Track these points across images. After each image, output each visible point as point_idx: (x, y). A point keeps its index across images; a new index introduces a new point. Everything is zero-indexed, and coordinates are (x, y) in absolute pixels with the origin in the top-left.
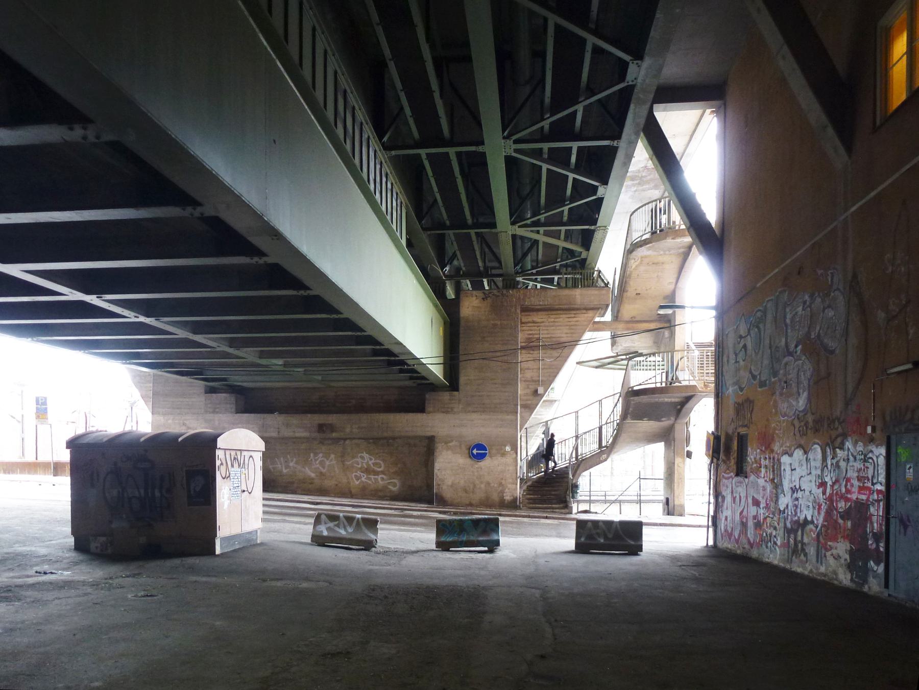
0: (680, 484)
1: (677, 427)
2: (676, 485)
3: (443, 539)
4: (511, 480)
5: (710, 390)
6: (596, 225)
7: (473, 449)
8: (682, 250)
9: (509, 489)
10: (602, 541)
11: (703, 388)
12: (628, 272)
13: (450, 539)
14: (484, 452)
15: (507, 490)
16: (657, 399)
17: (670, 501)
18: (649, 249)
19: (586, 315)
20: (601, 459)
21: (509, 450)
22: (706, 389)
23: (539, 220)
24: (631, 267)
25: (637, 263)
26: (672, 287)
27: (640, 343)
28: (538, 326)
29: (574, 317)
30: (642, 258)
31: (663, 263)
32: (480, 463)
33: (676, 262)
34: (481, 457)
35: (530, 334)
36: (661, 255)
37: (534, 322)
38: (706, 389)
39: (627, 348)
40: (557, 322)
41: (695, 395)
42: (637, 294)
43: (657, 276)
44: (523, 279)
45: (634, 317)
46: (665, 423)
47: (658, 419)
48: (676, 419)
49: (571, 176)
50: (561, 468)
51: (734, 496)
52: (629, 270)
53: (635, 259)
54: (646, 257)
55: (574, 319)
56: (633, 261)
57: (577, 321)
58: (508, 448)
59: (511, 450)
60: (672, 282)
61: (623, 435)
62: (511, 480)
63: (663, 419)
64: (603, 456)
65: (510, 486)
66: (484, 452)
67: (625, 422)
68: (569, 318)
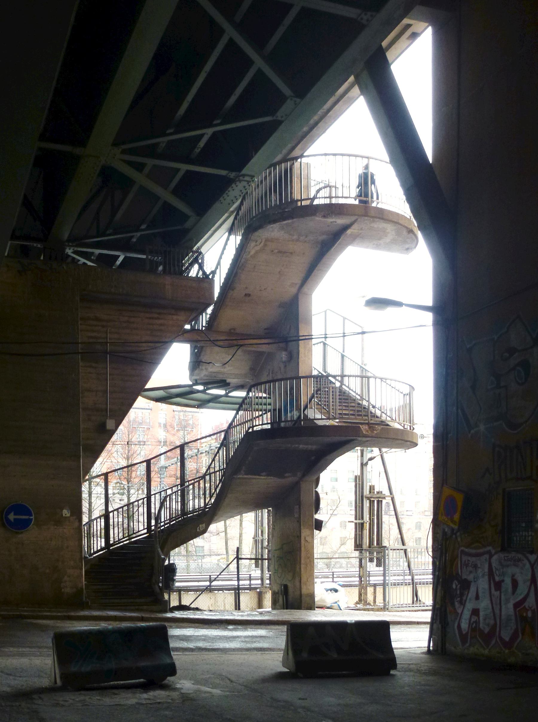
0: (308, 565)
1: (304, 486)
2: (303, 566)
3: (74, 669)
4: (72, 563)
5: (376, 434)
6: (240, 170)
7: (8, 513)
8: (324, 237)
9: (69, 576)
10: (335, 656)
11: (367, 431)
12: (243, 260)
13: (86, 668)
14: (27, 517)
15: (66, 578)
16: (289, 445)
17: (290, 590)
18: (282, 228)
19: (175, 317)
20: (198, 530)
21: (68, 515)
22: (372, 432)
23: (156, 145)
24: (249, 252)
25: (258, 248)
26: (294, 290)
27: (232, 368)
28: (103, 326)
29: (158, 318)
30: (267, 240)
31: (291, 253)
32: (20, 536)
33: (310, 253)
34: (23, 525)
35: (92, 337)
36: (293, 241)
37: (97, 319)
38: (372, 432)
39: (214, 375)
40: (133, 323)
41: (353, 440)
42: (246, 295)
43: (279, 272)
44: (75, 252)
45: (234, 329)
46: (289, 480)
47: (280, 475)
48: (304, 475)
49: (259, 63)
50: (124, 544)
51: (497, 579)
52: (244, 256)
53: (257, 241)
54: (272, 240)
55: (157, 322)
56: (253, 244)
57: (161, 325)
58: (66, 513)
59: (71, 515)
60: (296, 284)
61: (229, 495)
62: (72, 563)
63: (287, 475)
64: (200, 526)
65: (70, 571)
66: (27, 517)
67: (235, 476)
68: (150, 318)
